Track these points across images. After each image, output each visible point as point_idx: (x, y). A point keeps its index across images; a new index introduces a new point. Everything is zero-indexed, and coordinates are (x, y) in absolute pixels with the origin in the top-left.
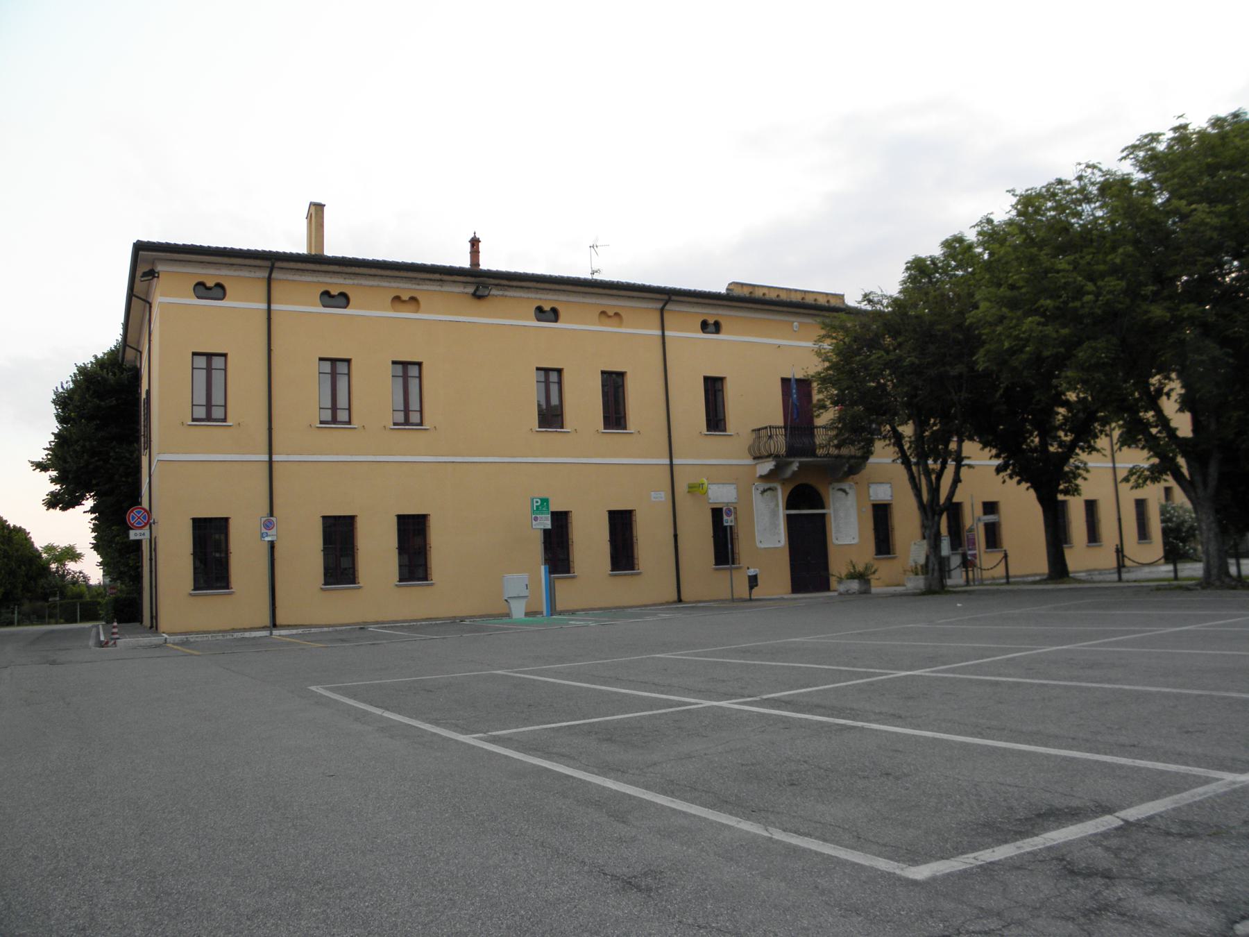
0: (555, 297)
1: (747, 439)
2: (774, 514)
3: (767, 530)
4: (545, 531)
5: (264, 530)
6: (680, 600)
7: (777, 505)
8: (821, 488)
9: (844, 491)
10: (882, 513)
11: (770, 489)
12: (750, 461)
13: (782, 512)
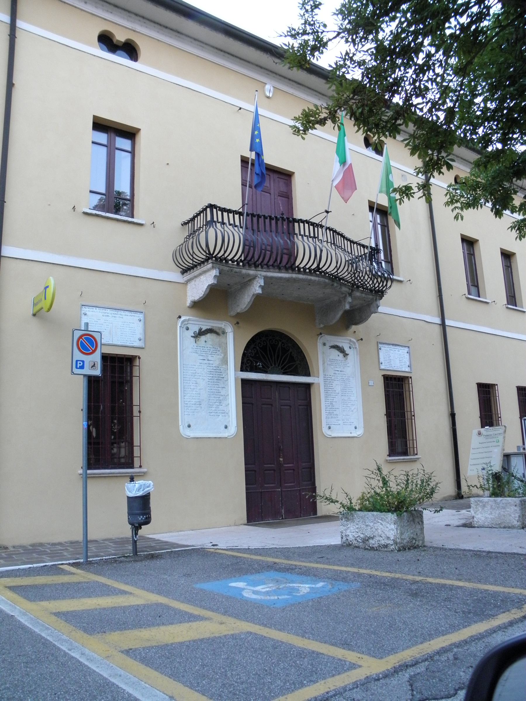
0: (138, 28)
1: (172, 235)
2: (218, 376)
3: (199, 400)
4: (92, 381)
5: (78, 356)
6: (459, 496)
7: (225, 361)
8: (304, 341)
9: (341, 350)
10: (396, 389)
11: (210, 331)
12: (175, 276)
13: (233, 375)
